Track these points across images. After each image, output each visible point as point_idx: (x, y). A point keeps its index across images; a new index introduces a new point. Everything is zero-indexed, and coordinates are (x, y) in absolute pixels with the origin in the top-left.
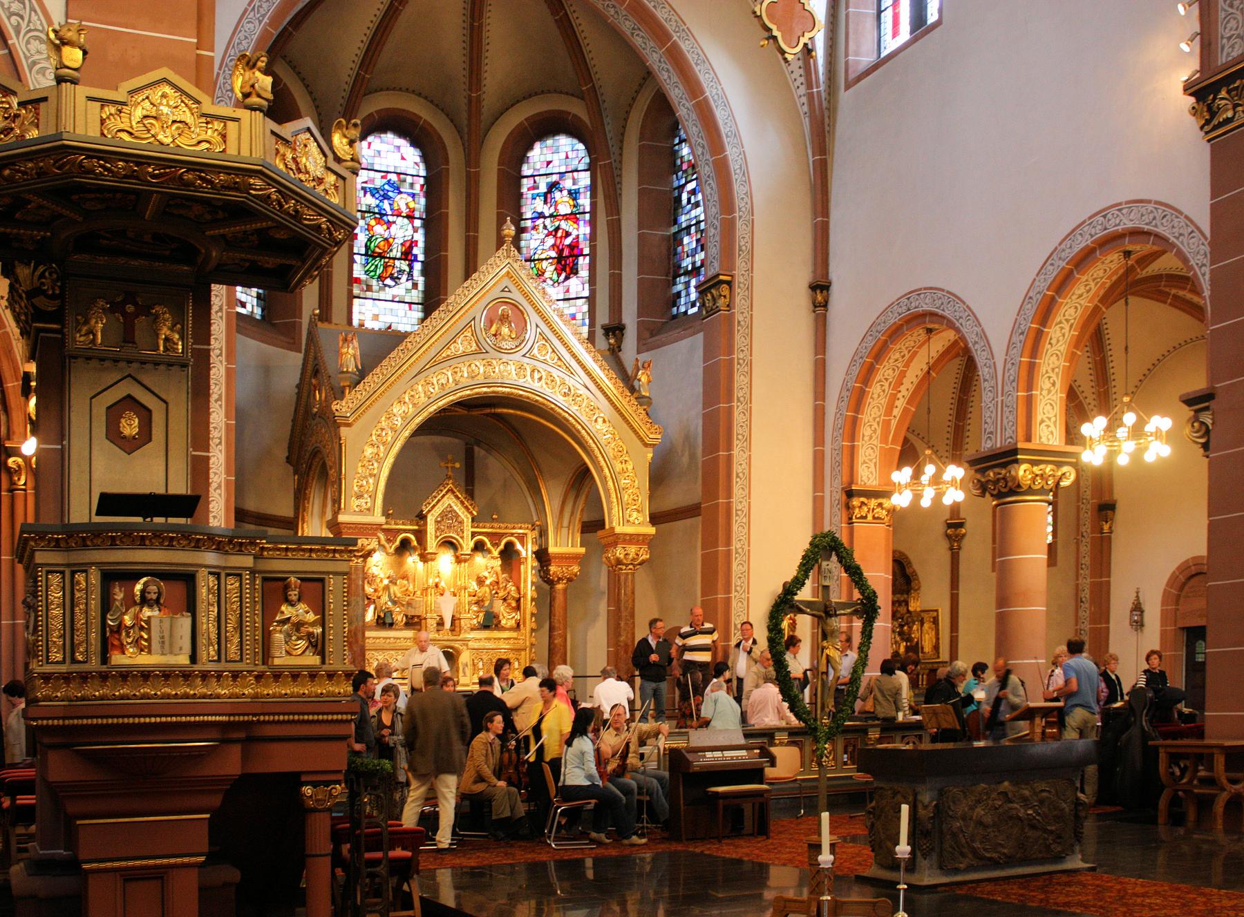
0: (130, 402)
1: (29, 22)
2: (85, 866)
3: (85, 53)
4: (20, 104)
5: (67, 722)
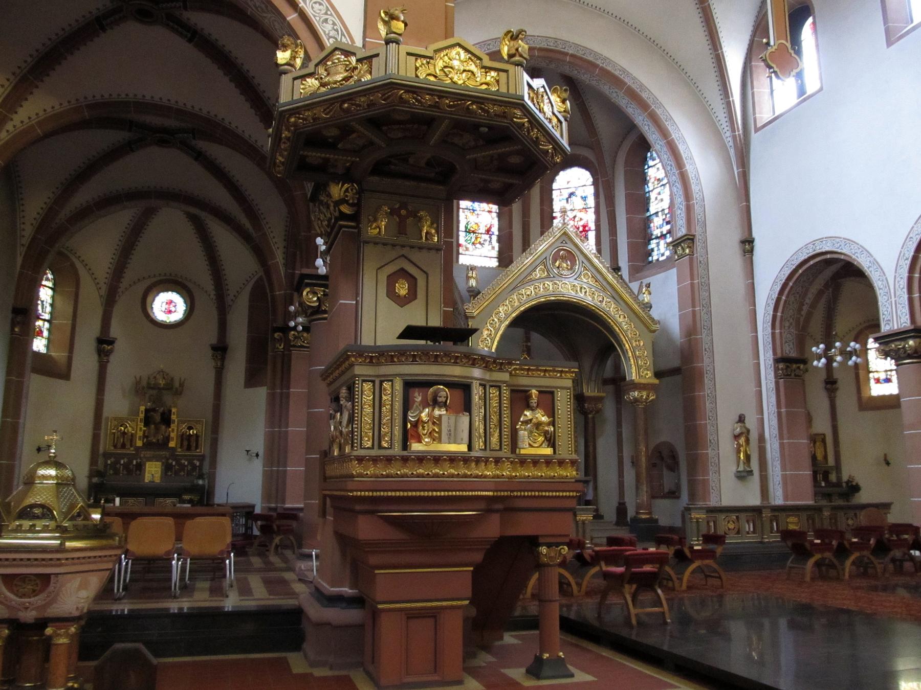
2: (380, 606)
3: (406, 25)
4: (358, 61)
5: (375, 494)
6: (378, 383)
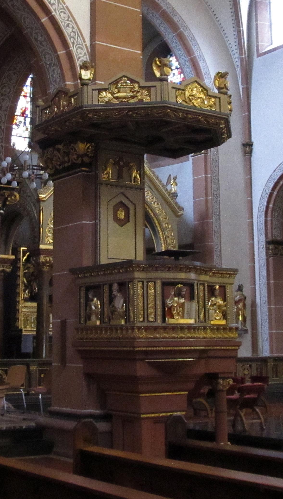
0: (121, 204)
1: (77, 41)
2: (143, 416)
5: (148, 349)
6: (145, 283)
